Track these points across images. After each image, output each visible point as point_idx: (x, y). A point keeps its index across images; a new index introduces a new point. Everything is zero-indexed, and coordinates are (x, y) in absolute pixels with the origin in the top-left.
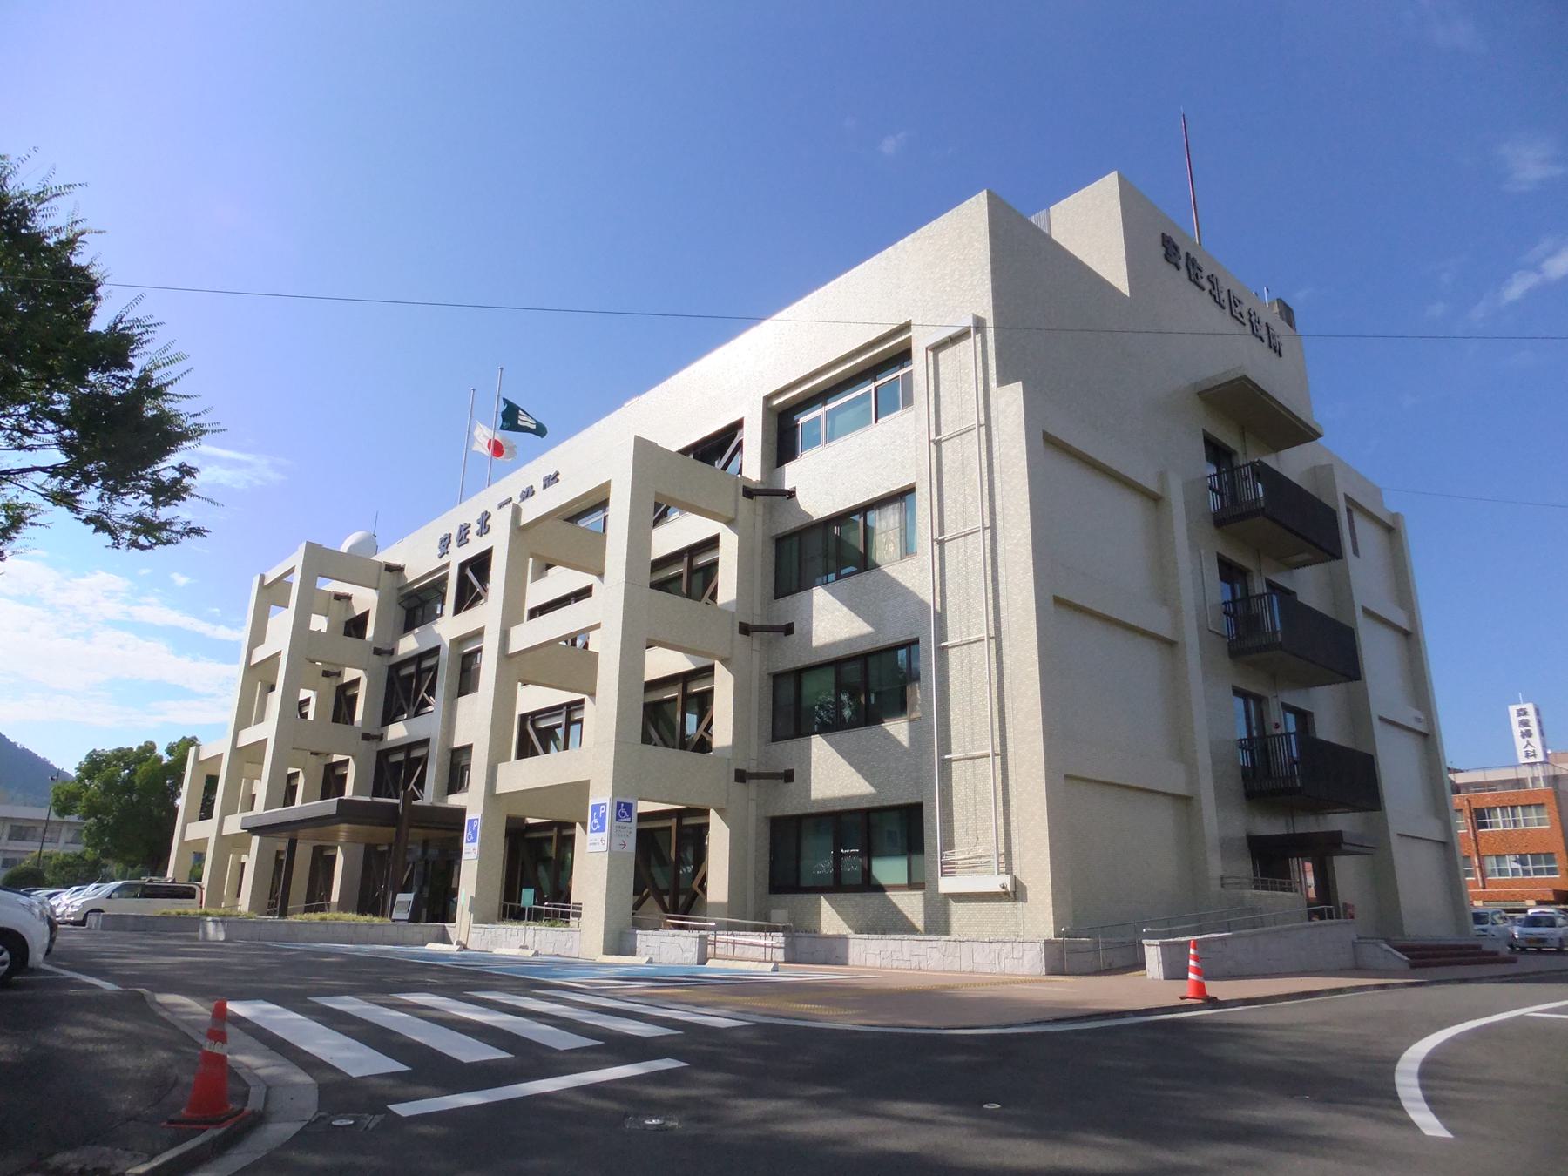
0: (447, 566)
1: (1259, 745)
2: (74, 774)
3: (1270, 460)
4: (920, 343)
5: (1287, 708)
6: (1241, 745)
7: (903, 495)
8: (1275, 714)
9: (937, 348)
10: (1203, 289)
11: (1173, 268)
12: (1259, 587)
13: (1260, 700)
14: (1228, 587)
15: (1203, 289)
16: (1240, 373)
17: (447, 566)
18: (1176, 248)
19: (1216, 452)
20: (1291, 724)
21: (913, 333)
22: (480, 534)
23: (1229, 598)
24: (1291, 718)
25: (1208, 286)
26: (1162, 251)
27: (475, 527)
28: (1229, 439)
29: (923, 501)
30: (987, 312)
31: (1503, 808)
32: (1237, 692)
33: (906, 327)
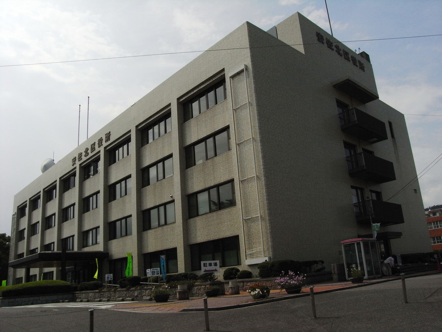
0: (75, 168)
1: (362, 204)
2: (426, 207)
3: (361, 108)
4: (228, 75)
5: (372, 191)
6: (355, 205)
7: (227, 128)
8: (367, 194)
9: (233, 77)
10: (333, 50)
11: (355, 66)
12: (359, 150)
13: (362, 190)
14: (348, 151)
15: (333, 50)
16: (347, 78)
17: (75, 168)
18: (322, 36)
19: (340, 104)
20: (374, 197)
21: (226, 72)
22: (86, 156)
23: (349, 155)
24: (374, 195)
25: (335, 49)
26: (317, 38)
27: (84, 154)
28: (345, 100)
29: (232, 130)
30: (248, 62)
31: (434, 222)
32: (352, 187)
33: (223, 70)
